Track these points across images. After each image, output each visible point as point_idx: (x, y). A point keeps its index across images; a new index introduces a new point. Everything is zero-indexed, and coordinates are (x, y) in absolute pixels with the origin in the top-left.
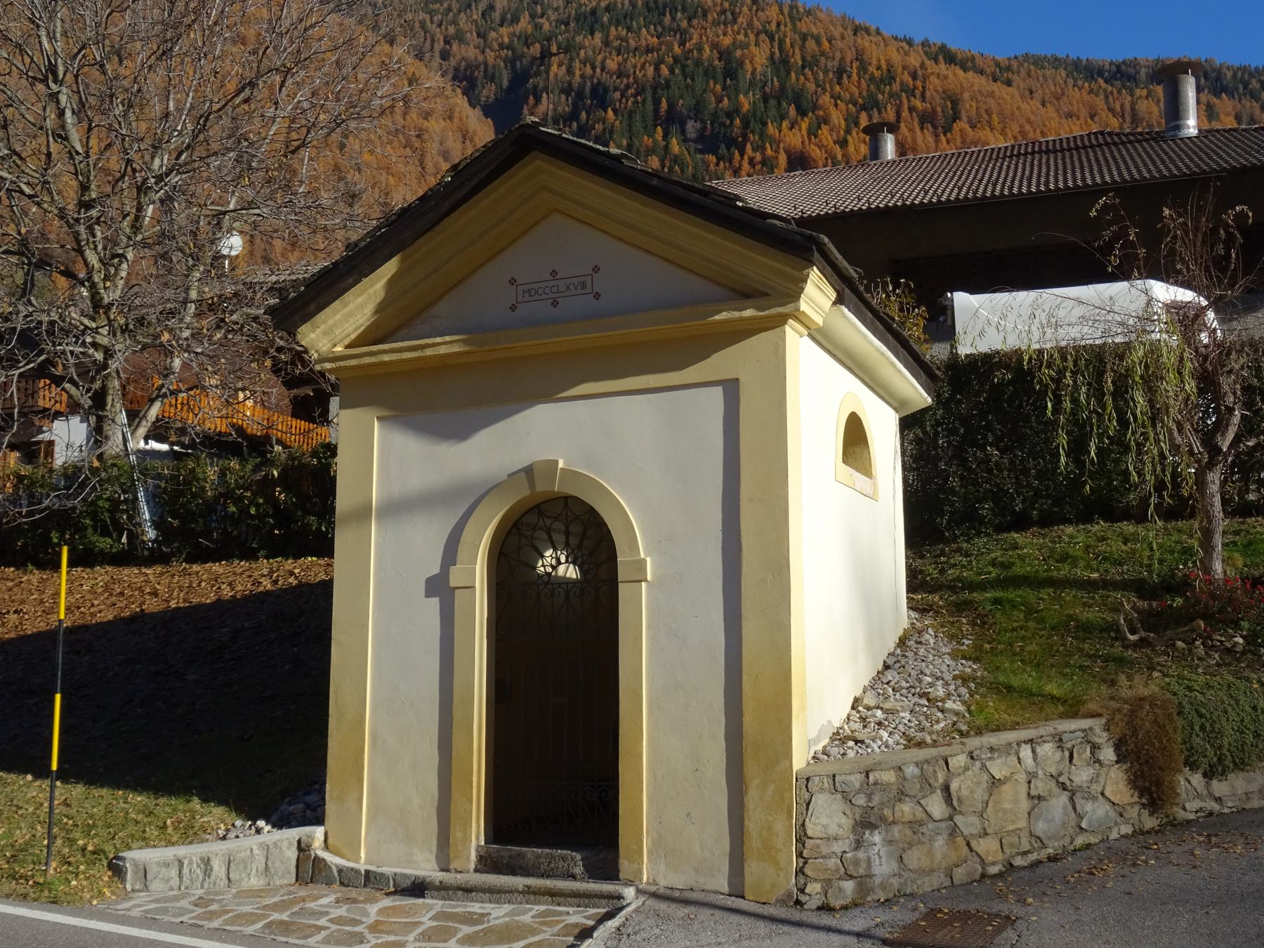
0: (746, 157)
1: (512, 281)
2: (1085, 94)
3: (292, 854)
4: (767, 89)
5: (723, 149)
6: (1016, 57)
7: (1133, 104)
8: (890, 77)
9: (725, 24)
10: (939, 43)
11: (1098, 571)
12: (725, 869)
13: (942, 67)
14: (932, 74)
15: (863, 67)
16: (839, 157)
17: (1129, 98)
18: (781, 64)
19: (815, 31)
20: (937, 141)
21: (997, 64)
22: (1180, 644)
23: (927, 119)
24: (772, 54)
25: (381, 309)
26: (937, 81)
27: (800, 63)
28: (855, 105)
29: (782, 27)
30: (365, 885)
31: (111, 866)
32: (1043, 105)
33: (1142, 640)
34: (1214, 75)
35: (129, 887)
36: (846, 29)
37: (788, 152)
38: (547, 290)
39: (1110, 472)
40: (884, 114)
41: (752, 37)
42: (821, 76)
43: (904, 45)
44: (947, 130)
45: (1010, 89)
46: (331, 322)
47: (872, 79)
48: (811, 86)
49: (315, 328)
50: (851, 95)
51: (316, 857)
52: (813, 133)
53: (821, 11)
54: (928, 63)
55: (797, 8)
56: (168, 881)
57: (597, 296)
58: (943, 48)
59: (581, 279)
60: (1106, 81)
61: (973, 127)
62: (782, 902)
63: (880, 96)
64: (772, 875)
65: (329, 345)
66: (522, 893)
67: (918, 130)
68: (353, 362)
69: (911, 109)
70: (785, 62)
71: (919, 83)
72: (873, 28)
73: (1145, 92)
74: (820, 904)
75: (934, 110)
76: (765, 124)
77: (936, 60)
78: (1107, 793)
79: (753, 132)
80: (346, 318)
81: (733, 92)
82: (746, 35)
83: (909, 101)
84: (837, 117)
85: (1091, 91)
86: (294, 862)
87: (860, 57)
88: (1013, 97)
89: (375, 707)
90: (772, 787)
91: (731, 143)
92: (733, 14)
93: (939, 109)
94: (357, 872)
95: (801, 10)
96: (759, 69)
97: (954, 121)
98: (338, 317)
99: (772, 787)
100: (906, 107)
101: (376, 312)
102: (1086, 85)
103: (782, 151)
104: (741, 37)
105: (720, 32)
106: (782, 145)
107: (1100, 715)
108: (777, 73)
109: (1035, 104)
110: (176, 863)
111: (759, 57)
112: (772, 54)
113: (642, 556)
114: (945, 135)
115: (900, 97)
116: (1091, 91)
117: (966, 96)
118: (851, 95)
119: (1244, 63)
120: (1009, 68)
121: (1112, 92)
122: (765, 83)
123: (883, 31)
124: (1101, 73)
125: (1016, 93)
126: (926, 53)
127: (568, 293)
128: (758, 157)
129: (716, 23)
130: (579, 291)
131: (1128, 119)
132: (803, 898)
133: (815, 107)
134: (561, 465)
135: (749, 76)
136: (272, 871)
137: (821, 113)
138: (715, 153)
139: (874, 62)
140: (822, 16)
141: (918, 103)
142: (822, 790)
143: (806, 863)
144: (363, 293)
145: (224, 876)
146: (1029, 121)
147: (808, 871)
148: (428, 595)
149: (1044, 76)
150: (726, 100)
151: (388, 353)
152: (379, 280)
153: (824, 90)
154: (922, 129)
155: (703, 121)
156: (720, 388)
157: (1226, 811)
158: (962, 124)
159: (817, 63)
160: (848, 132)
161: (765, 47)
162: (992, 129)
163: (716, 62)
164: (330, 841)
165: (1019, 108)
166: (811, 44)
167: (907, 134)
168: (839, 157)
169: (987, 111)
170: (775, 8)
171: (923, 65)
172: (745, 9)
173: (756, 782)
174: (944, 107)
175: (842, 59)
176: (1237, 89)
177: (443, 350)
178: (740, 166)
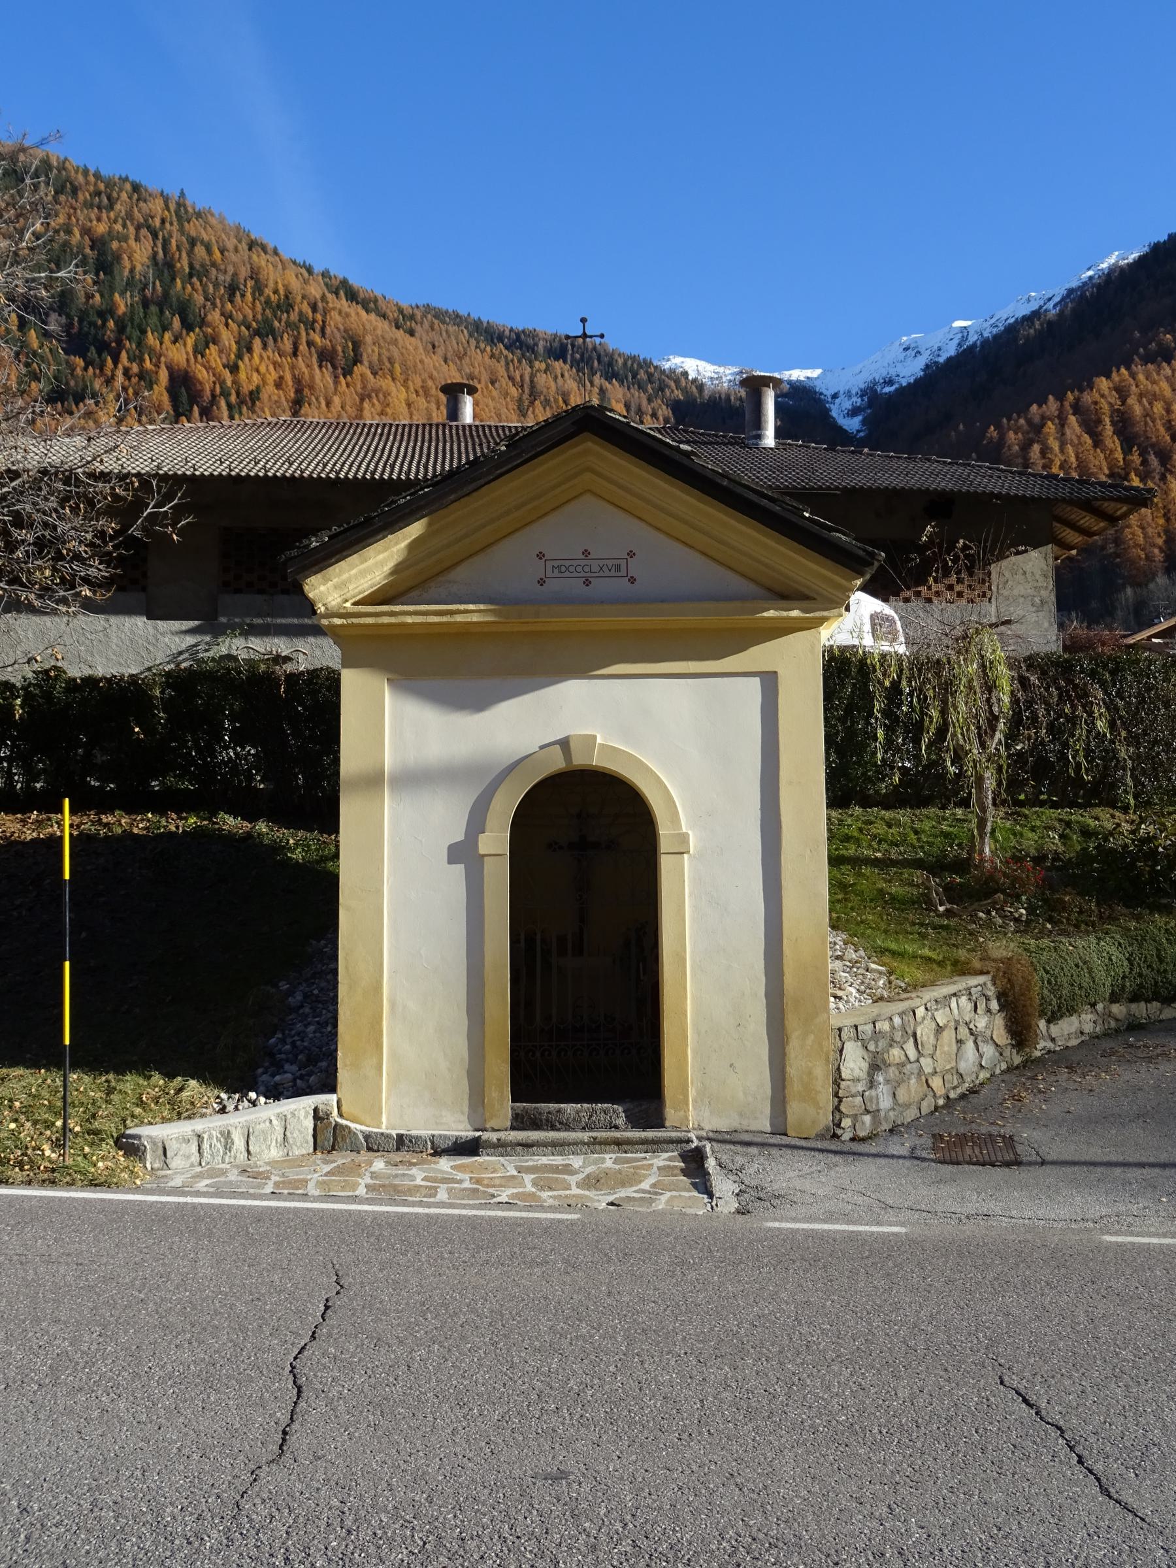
0: (120, 366)
1: (541, 555)
2: (487, 358)
3: (309, 1123)
4: (148, 293)
5: (92, 353)
6: (417, 307)
7: (532, 376)
8: (287, 304)
9: (99, 208)
10: (341, 277)
11: (879, 851)
12: (767, 1111)
13: (344, 303)
14: (334, 309)
15: (259, 288)
16: (229, 383)
17: (529, 369)
18: (165, 267)
19: (206, 238)
20: (336, 382)
21: (401, 311)
22: (981, 914)
23: (326, 357)
24: (155, 254)
25: (397, 570)
26: (338, 317)
27: (187, 270)
28: (248, 328)
29: (167, 225)
30: (398, 1149)
31: (118, 1144)
32: (446, 361)
33: (947, 910)
34: (606, 359)
35: (149, 1166)
36: (240, 241)
37: (169, 368)
38: (579, 569)
39: (866, 763)
40: (280, 344)
41: (132, 230)
42: (211, 290)
43: (304, 271)
44: (347, 372)
45: (412, 339)
46: (345, 576)
47: (268, 302)
48: (199, 299)
49: (326, 580)
50: (245, 316)
51: (337, 1124)
52: (199, 351)
53: (212, 215)
54: (330, 296)
55: (185, 206)
56: (188, 1157)
57: (632, 580)
58: (344, 283)
59: (618, 562)
60: (507, 348)
61: (375, 374)
62: (821, 1137)
63: (276, 324)
64: (809, 1113)
65: (339, 600)
66: (588, 1144)
67: (316, 367)
68: (370, 620)
69: (310, 344)
70: (169, 265)
71: (319, 317)
72: (271, 246)
73: (543, 366)
74: (851, 1135)
75: (334, 350)
76: (144, 332)
77: (337, 294)
78: (995, 1037)
79: (129, 339)
80: (363, 573)
81: (107, 289)
82: (124, 226)
83: (308, 334)
84: (228, 338)
85: (492, 356)
86: (311, 1131)
87: (255, 275)
88: (416, 348)
89: (394, 972)
90: (812, 1037)
91: (103, 347)
92: (109, 198)
93: (339, 349)
94: (388, 1136)
95: (190, 210)
96: (139, 268)
97: (355, 363)
98: (353, 572)
99: (812, 1037)
100: (304, 340)
101: (392, 573)
102: (488, 348)
103: (163, 366)
104: (118, 227)
105: (93, 217)
106: (163, 359)
107: (988, 973)
108: (159, 275)
109: (437, 359)
110: (196, 1138)
111: (138, 255)
112: (155, 254)
113: (684, 830)
114: (345, 377)
115: (298, 328)
116: (492, 356)
117: (369, 339)
118: (245, 316)
119: (635, 353)
120: (412, 317)
121: (512, 361)
122: (145, 286)
123: (280, 251)
124: (501, 338)
125: (420, 344)
126: (326, 285)
127: (601, 574)
128: (135, 368)
129: (88, 205)
130: (613, 573)
131: (527, 391)
132: (839, 1132)
133: (203, 323)
134: (599, 741)
135: (126, 273)
136: (291, 1141)
137: (209, 330)
138: (83, 356)
139: (271, 285)
140: (213, 221)
141: (317, 338)
142: (850, 1039)
143: (840, 1101)
144: (386, 550)
145: (243, 1149)
146: (431, 377)
147: (842, 1108)
148: (450, 862)
149: (447, 331)
150: (98, 297)
151: (409, 615)
152: (405, 538)
153: (214, 305)
154: (320, 367)
155: (68, 316)
156: (757, 679)
157: (1058, 1049)
158: (361, 369)
159: (206, 273)
160: (239, 356)
161: (147, 243)
162: (393, 379)
163: (88, 251)
164: (344, 1109)
165: (421, 361)
166: (200, 251)
167: (304, 369)
168: (229, 383)
169: (389, 359)
170: (160, 202)
171: (323, 298)
172: (124, 196)
173: (797, 1033)
174: (345, 348)
175: (235, 274)
176: (626, 377)
177: (475, 618)
178: (113, 376)
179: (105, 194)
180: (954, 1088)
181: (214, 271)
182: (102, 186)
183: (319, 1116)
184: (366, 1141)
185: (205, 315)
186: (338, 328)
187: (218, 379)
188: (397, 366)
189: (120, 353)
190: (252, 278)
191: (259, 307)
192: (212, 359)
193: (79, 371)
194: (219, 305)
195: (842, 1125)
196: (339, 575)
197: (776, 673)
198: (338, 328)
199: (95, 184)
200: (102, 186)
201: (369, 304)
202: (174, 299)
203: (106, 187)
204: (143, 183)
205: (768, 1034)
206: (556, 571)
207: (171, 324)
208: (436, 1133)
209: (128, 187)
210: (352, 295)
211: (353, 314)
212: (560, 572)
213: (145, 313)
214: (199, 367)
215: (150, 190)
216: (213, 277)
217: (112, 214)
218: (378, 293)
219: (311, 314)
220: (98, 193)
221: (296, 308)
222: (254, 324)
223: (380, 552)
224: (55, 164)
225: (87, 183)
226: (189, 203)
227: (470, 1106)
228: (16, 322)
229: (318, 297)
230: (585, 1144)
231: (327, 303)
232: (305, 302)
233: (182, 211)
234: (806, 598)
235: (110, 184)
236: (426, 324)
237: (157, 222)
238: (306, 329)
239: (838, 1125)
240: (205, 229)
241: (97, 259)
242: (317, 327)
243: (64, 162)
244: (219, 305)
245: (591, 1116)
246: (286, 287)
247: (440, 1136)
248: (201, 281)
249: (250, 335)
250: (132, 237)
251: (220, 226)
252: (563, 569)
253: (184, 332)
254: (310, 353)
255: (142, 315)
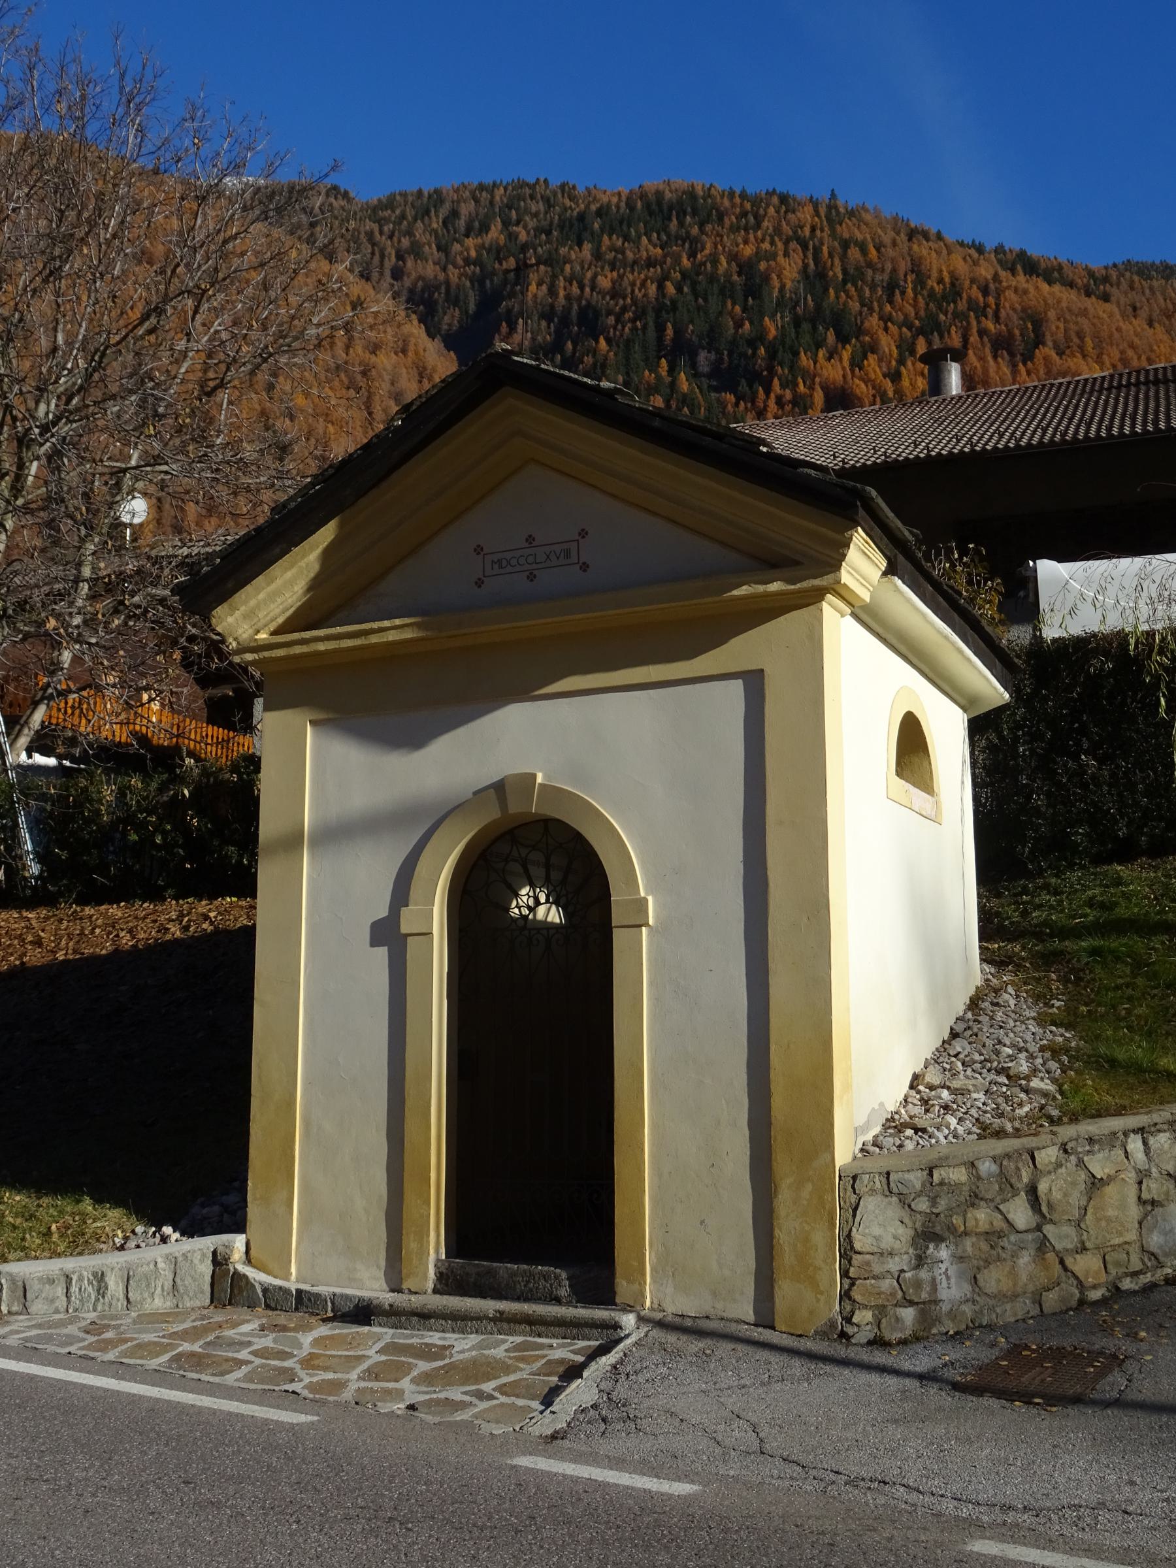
0: (772, 395)
1: (479, 550)
3: (206, 1269)
4: (799, 310)
5: (743, 386)
8: (954, 291)
9: (746, 230)
10: (1018, 249)
13: (1021, 279)
14: (1009, 287)
15: (921, 280)
18: (816, 279)
19: (860, 237)
21: (1091, 274)
24: (806, 266)
25: (315, 585)
26: (1013, 295)
27: (841, 277)
28: (910, 329)
29: (818, 232)
30: (297, 1309)
32: (1150, 324)
36: (898, 233)
41: (780, 245)
42: (867, 293)
43: (973, 252)
44: (1028, 357)
45: (1107, 305)
46: (253, 603)
47: (932, 294)
48: (855, 306)
49: (234, 609)
51: (236, 1272)
52: (857, 363)
53: (867, 211)
54: (1003, 274)
55: (836, 207)
56: (52, 1301)
58: (1022, 255)
61: (1061, 354)
62: (822, 1334)
63: (942, 317)
64: (811, 1300)
65: (251, 631)
67: (990, 358)
69: (982, 333)
70: (821, 275)
71: (991, 300)
72: (934, 231)
74: (871, 1336)
76: (796, 354)
77: (1013, 271)
79: (781, 364)
80: (272, 597)
82: (772, 243)
83: (979, 322)
84: (888, 344)
86: (208, 1279)
88: (1111, 316)
89: (308, 1083)
90: (809, 1187)
92: (755, 218)
93: (1017, 332)
95: (842, 210)
96: (789, 285)
98: (261, 596)
99: (809, 1187)
100: (975, 330)
103: (818, 387)
104: (766, 246)
105: (740, 240)
109: (1139, 323)
110: (63, 1279)
111: (789, 270)
112: (806, 266)
113: (643, 894)
114: (1025, 364)
115: (967, 318)
117: (1052, 314)
118: (906, 316)
120: (1106, 279)
122: (797, 303)
125: (1116, 310)
126: (1000, 262)
128: (788, 394)
129: (734, 229)
132: (850, 1330)
133: (860, 331)
135: (776, 293)
137: (867, 338)
138: (733, 391)
139: (935, 274)
140: (867, 217)
141: (990, 325)
142: (873, 1191)
143: (853, 1284)
146: (1132, 346)
147: (856, 1295)
148: (374, 943)
149: (1151, 288)
150: (747, 325)
151: (324, 641)
152: (312, 549)
153: (871, 310)
154: (995, 357)
156: (740, 681)
160: (901, 362)
161: (797, 258)
162: (1084, 356)
163: (735, 277)
165: (1119, 329)
166: (854, 253)
170: (809, 209)
171: (996, 277)
172: (771, 210)
174: (1023, 330)
175: (894, 270)
177: (392, 636)
178: (766, 407)
179: (751, 212)
180: (1135, 1274)
181: (870, 272)
182: (748, 206)
183: (219, 1261)
184: (264, 1296)
185: (862, 323)
186: (1014, 309)
187: (878, 391)
188: (1088, 340)
189: (772, 381)
190: (913, 271)
191: (921, 302)
192: (870, 369)
193: (730, 408)
194: (876, 308)
195: (854, 1320)
196: (245, 603)
197: (762, 671)
198: (1014, 309)
199: (742, 205)
200: (748, 206)
201: (1051, 273)
202: (827, 312)
203: (752, 206)
204: (791, 193)
205: (751, 1178)
206: (496, 566)
207: (825, 339)
208: (338, 1290)
209: (775, 200)
210: (1030, 266)
211: (1032, 290)
212: (501, 567)
213: (797, 333)
214: (857, 381)
215: (799, 197)
216: (869, 279)
217: (759, 233)
218: (1062, 259)
219: (981, 299)
220: (745, 214)
221: (964, 295)
222: (917, 322)
223: (287, 569)
224: (701, 193)
225: (733, 206)
226: (840, 202)
227: (388, 1259)
228: (666, 368)
229: (989, 277)
230: (491, 1319)
231: (1000, 282)
232: (975, 287)
233: (833, 214)
234: (797, 563)
235: (756, 201)
236: (1124, 285)
237: (807, 231)
238: (977, 318)
239: (848, 1320)
240: (859, 227)
241: (745, 285)
242: (990, 312)
243: (709, 189)
244: (876, 308)
245: (528, 1282)
246: (952, 274)
247: (342, 1296)
248: (856, 286)
249: (913, 336)
250: (781, 253)
251: (876, 221)
252: (504, 563)
253: (840, 346)
254: (982, 343)
255: (793, 335)
